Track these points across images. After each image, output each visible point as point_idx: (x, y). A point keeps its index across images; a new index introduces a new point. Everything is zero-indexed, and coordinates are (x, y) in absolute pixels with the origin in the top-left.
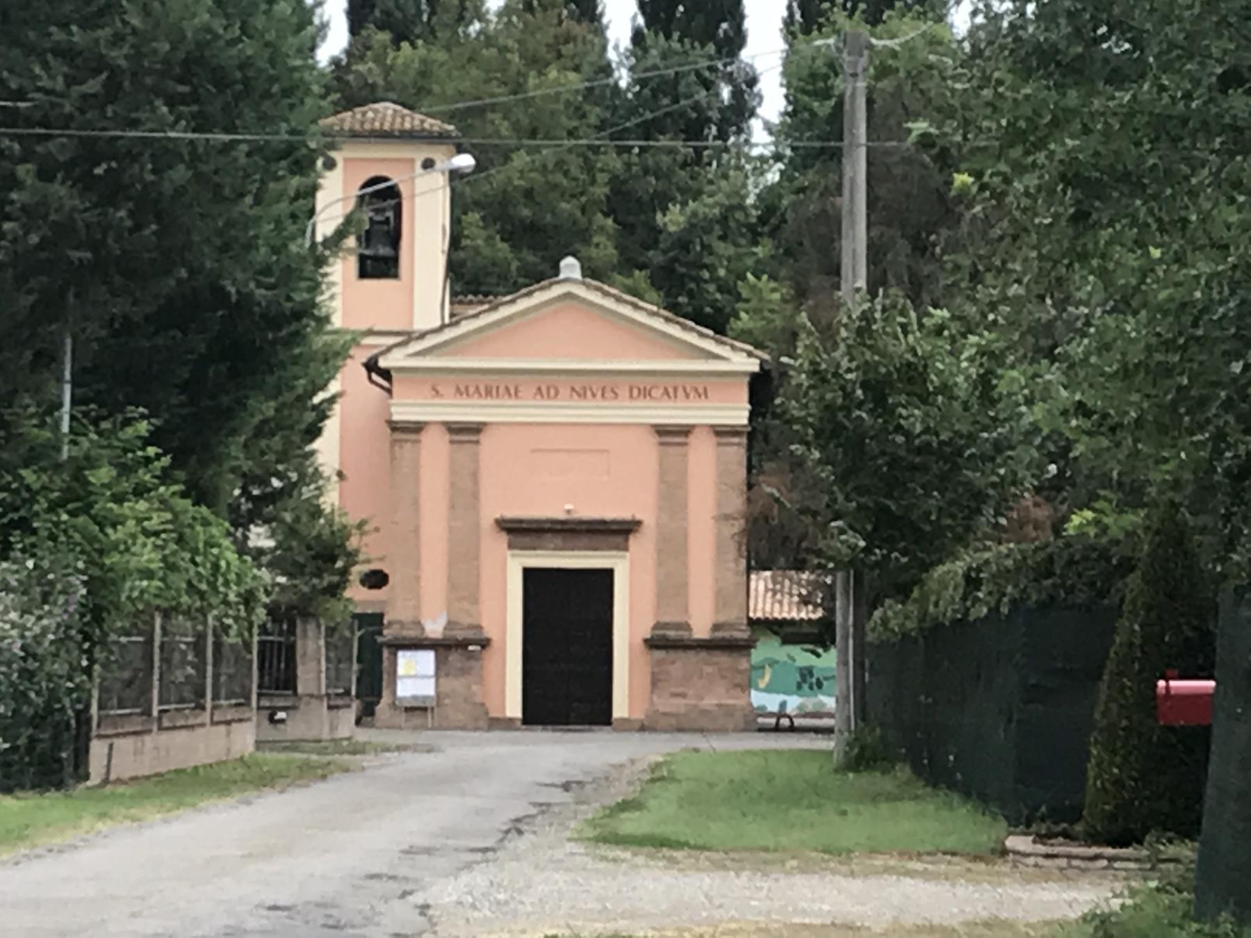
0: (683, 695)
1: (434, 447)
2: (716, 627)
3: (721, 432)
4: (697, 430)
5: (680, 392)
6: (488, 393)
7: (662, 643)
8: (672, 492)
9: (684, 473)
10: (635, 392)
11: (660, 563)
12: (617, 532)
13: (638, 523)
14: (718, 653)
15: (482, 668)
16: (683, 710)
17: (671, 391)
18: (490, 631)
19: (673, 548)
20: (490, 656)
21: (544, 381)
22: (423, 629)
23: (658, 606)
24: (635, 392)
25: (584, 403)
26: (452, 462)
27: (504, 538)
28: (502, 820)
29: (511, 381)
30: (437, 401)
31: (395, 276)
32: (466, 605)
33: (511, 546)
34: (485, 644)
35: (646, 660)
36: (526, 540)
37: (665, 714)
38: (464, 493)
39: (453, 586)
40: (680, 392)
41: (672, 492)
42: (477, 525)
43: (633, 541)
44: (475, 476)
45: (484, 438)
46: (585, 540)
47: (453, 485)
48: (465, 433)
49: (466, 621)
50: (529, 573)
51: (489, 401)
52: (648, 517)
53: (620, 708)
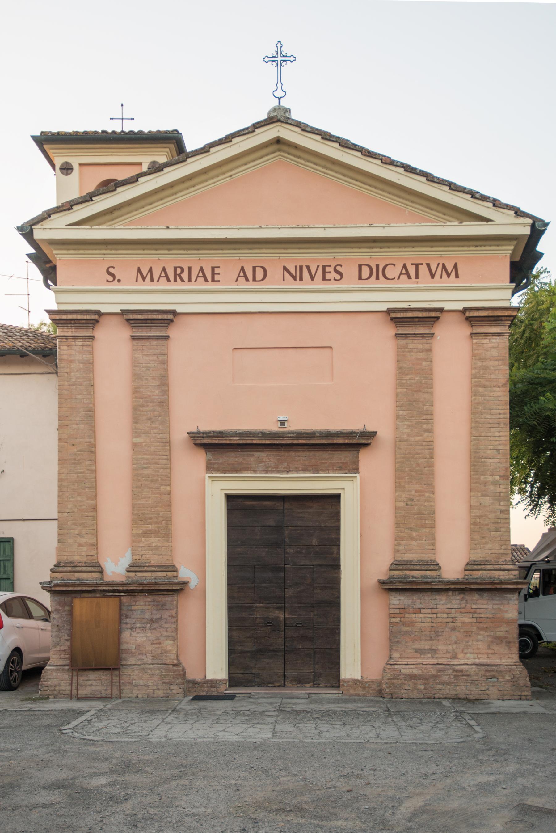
0: (434, 651)
1: (113, 348)
2: (471, 565)
3: (474, 318)
4: (445, 318)
5: (423, 270)
6: (177, 276)
7: (407, 583)
8: (414, 397)
9: (427, 375)
10: (366, 272)
11: (398, 486)
12: (347, 446)
13: (373, 434)
14: (475, 596)
15: (175, 617)
16: (433, 671)
17: (412, 270)
18: (185, 573)
19: (415, 470)
20: (187, 607)
21: (249, 258)
22: (101, 571)
23: (398, 539)
24: (366, 272)
25: (298, 285)
26: (135, 363)
27: (201, 458)
28: (445, 696)
29: (208, 259)
30: (115, 286)
31: (543, 254)
32: (155, 541)
33: (210, 467)
34: (178, 589)
35: (379, 607)
36: (232, 458)
37: (412, 677)
38: (151, 401)
39: (139, 516)
40: (423, 270)
41: (414, 397)
42: (168, 443)
43: (365, 458)
44: (164, 382)
45: (173, 332)
46: (302, 456)
47: (136, 391)
48: (151, 325)
49: (155, 560)
50: (232, 500)
51: (179, 286)
52: (385, 430)
53: (351, 667)
